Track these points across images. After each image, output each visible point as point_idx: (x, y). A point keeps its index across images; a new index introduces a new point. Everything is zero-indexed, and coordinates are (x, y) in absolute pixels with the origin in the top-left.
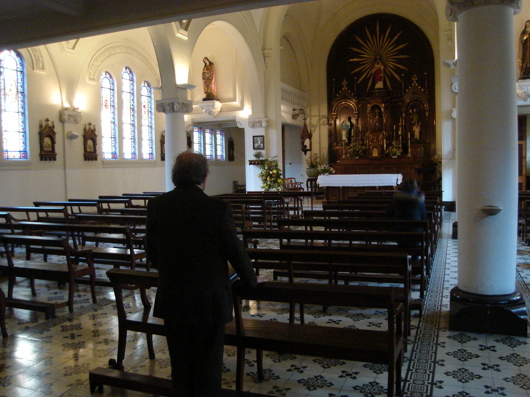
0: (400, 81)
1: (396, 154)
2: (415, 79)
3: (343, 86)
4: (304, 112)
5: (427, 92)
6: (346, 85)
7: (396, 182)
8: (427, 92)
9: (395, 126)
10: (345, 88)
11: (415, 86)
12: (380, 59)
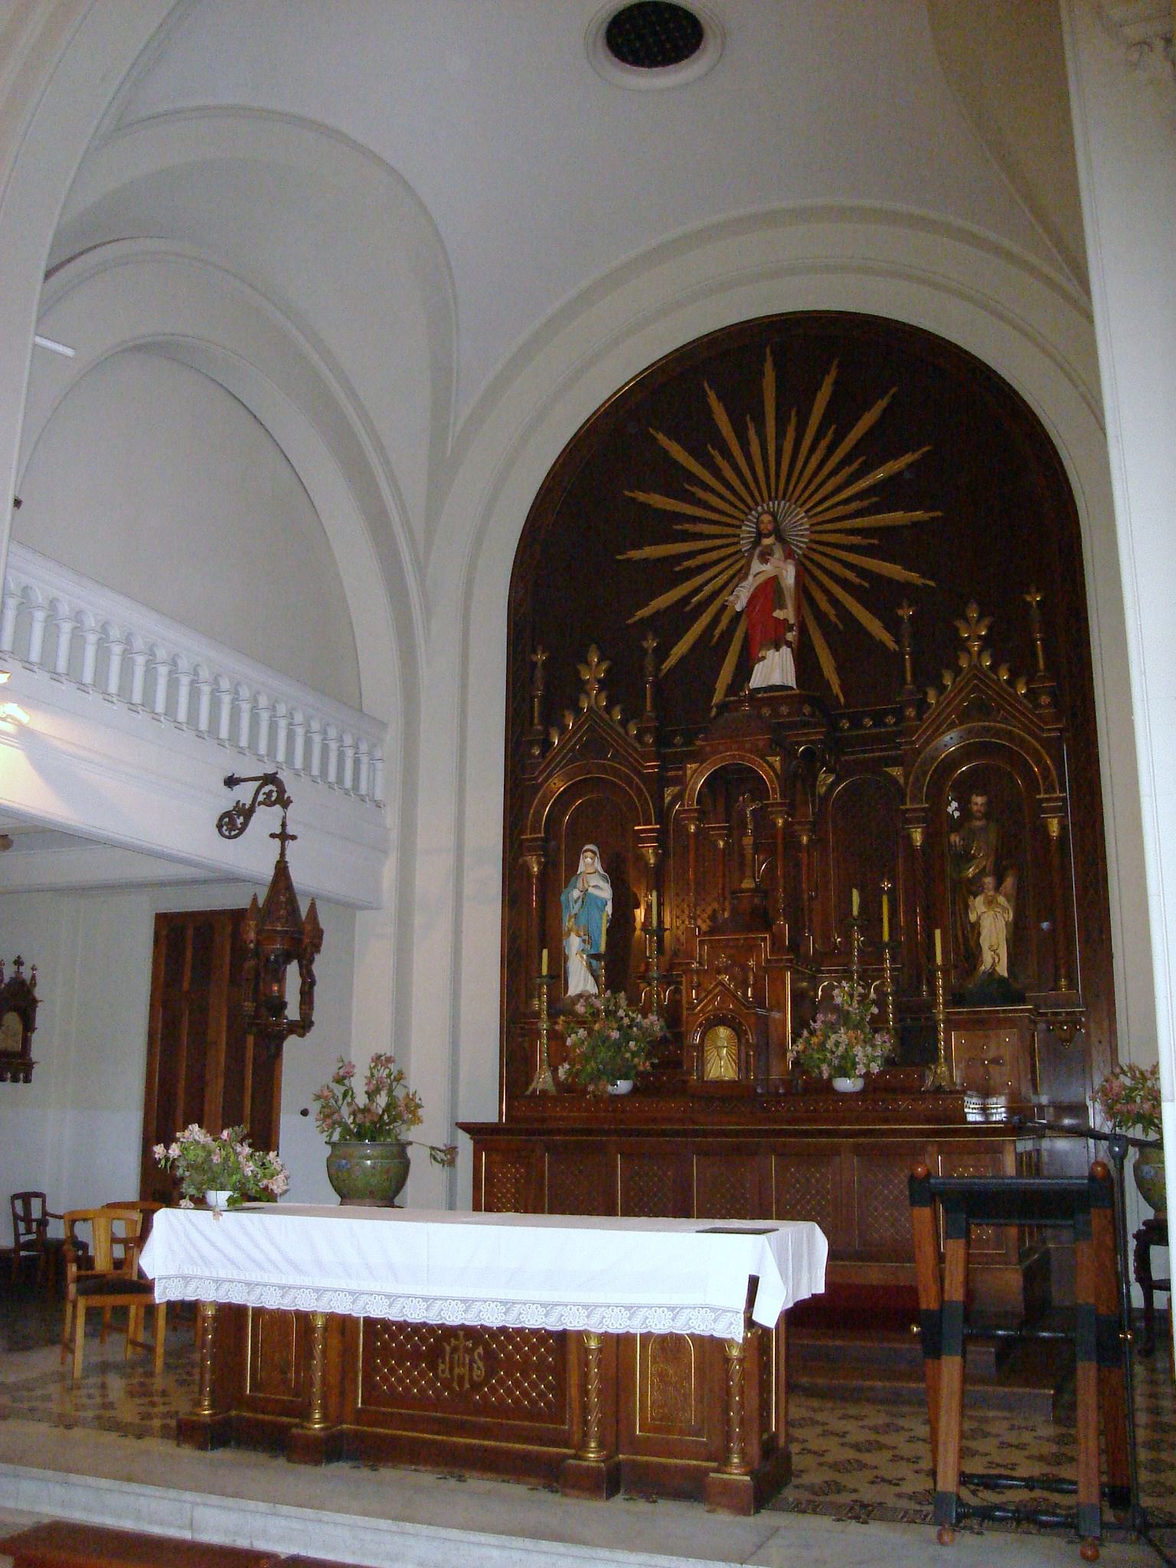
0: (892, 645)
1: (854, 1065)
2: (974, 629)
3: (581, 686)
4: (281, 791)
5: (1045, 700)
6: (599, 681)
7: (742, 1305)
8: (1045, 700)
9: (855, 894)
10: (593, 699)
11: (976, 667)
12: (778, 534)
